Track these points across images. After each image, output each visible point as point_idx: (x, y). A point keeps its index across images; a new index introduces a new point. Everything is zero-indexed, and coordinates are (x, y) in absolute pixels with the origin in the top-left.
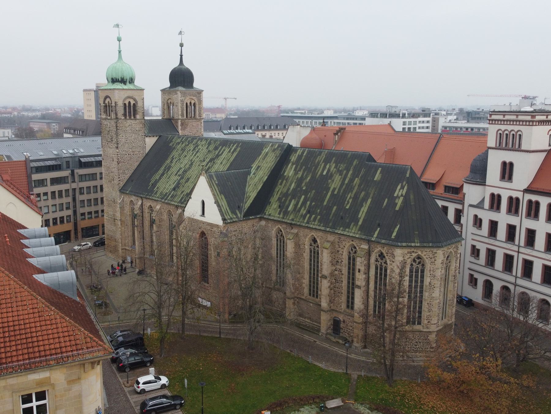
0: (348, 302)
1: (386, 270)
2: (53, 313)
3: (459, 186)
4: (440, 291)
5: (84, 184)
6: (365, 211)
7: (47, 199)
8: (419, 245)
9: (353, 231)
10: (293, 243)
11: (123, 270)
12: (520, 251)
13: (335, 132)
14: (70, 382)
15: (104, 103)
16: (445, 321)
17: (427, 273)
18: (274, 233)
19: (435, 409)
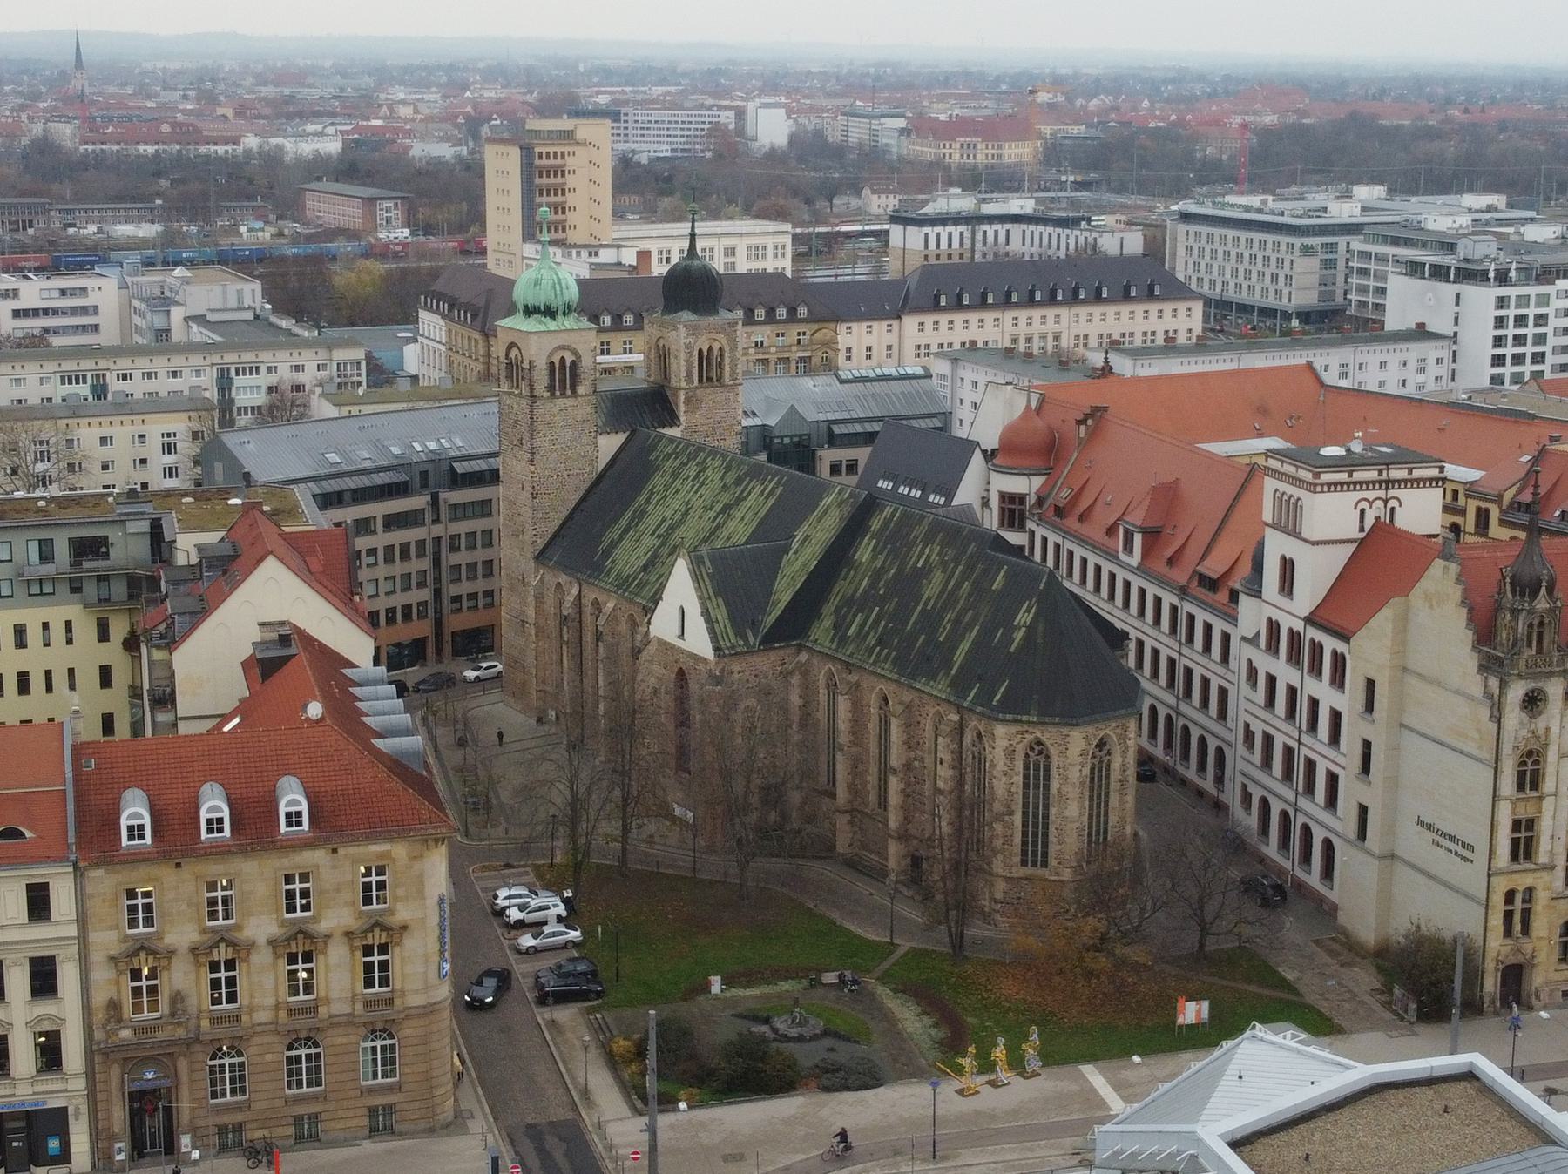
2: (396, 783)
5: (461, 528)
7: (376, 564)
13: (1081, 417)
14: (413, 858)
17: (1054, 772)
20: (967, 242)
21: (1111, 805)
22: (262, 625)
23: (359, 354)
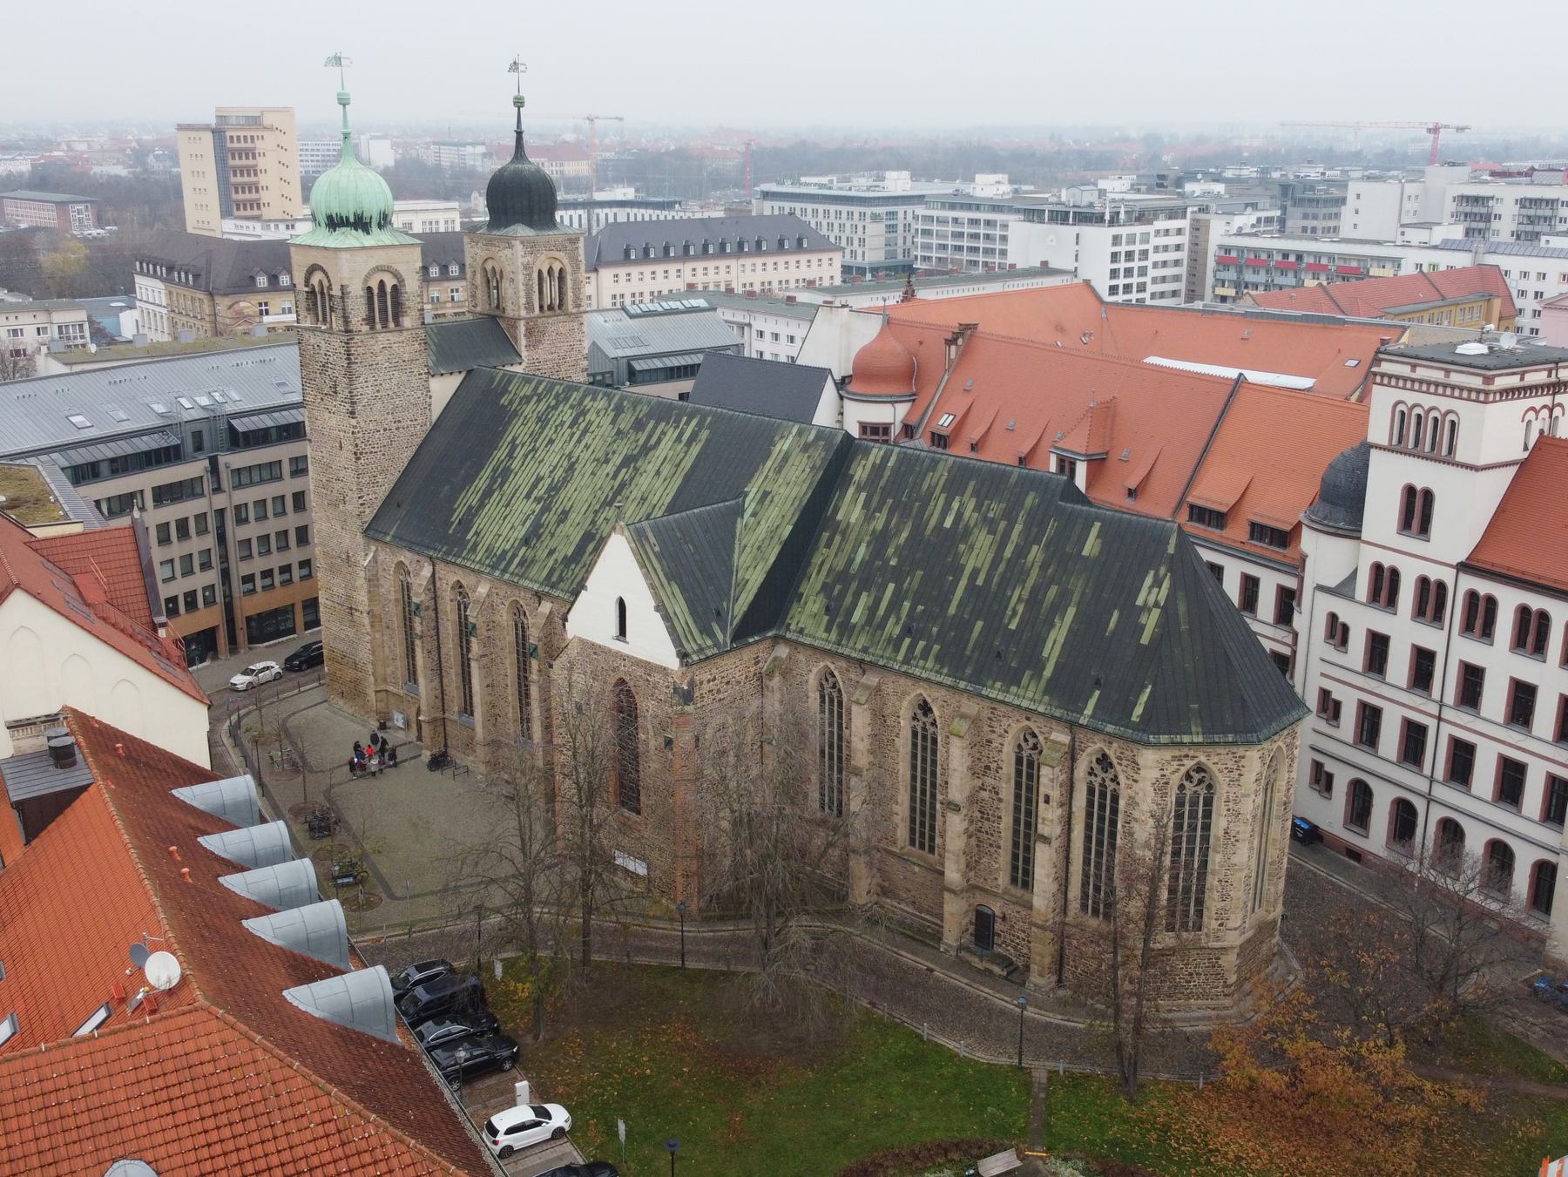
0: (1015, 868)
1: (1115, 799)
3: (1288, 528)
4: (1251, 849)
6: (1061, 640)
8: (1200, 739)
9: (1030, 694)
10: (868, 713)
11: (389, 756)
12: (1443, 716)
13: (949, 336)
15: (307, 283)
16: (1260, 913)
17: (1219, 807)
18: (812, 679)
19: (1243, 1163)
20: (585, 222)
21: (1272, 836)
22: (15, 726)
23: (81, 316)
